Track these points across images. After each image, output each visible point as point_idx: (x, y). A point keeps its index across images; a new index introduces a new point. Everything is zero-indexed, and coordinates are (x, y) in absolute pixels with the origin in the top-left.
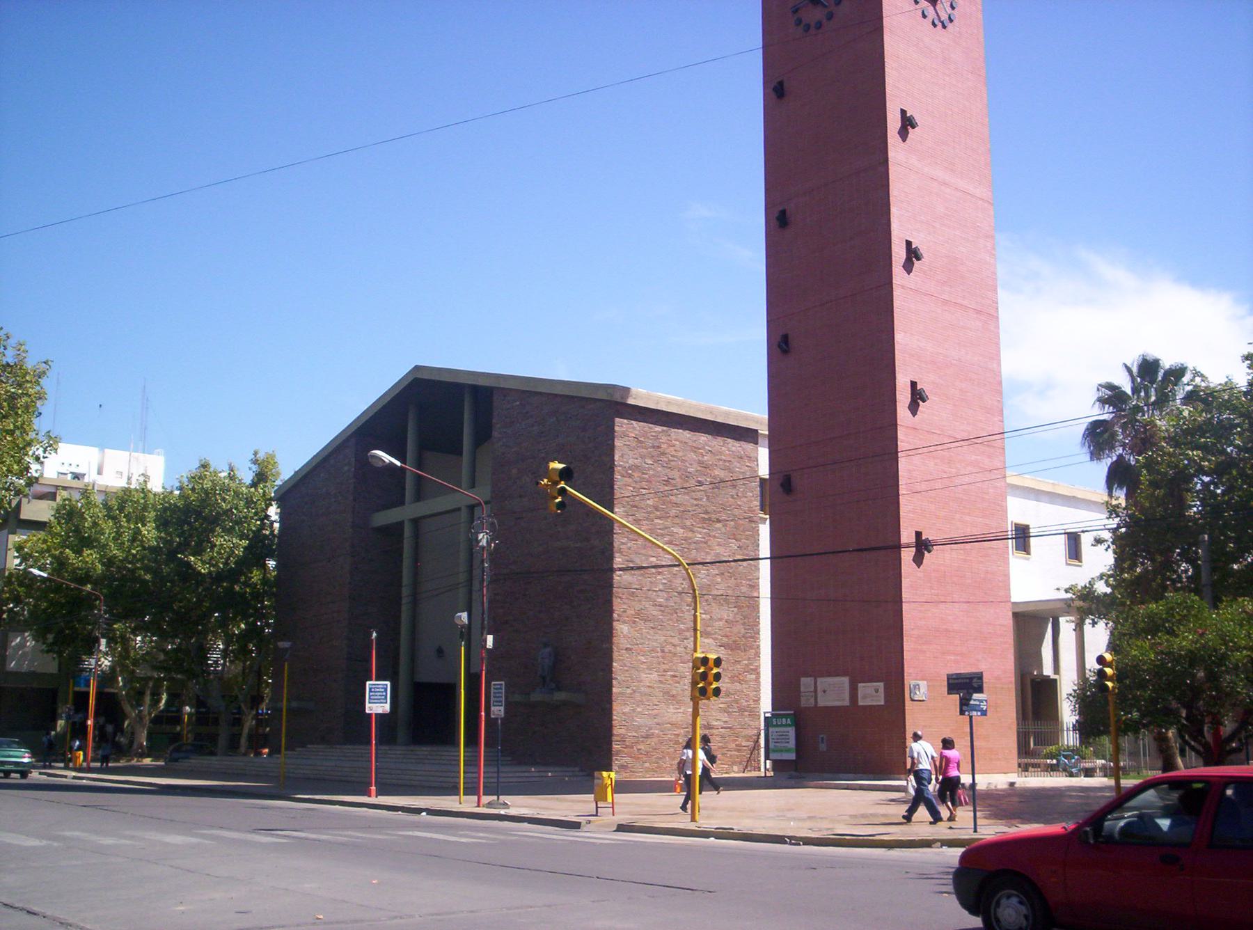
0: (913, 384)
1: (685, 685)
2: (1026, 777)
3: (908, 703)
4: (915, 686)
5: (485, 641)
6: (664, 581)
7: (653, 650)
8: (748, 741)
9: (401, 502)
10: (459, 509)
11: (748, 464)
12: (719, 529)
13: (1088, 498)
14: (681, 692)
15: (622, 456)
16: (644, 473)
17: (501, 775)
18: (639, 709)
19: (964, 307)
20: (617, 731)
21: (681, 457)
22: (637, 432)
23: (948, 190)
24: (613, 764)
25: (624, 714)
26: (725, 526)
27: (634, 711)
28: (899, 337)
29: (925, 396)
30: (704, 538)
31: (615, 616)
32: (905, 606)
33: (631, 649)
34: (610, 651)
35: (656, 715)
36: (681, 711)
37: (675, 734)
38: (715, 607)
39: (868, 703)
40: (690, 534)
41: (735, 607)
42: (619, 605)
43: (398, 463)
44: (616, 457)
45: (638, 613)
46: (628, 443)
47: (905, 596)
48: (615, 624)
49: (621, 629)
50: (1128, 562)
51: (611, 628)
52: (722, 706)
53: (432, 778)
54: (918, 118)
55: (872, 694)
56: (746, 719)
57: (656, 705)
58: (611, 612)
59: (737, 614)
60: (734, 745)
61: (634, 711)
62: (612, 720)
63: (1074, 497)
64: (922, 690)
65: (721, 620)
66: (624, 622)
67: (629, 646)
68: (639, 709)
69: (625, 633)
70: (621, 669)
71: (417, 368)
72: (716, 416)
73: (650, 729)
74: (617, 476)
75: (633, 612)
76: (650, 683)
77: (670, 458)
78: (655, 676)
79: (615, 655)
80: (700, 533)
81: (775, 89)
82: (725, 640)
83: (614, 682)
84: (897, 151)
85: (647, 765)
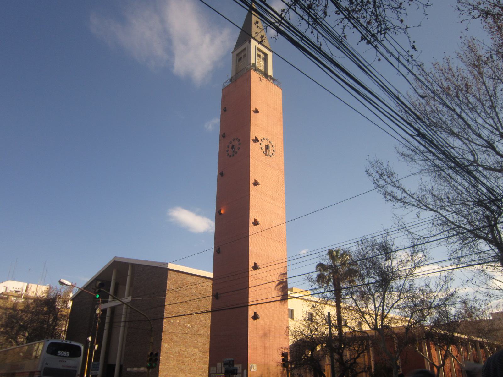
4: (252, 366)
6: (181, 329)
28: (250, 248)
31: (162, 340)
32: (249, 338)
38: (199, 339)
42: (164, 337)
47: (249, 334)
52: (200, 373)
65: (201, 342)
66: (166, 343)
71: (115, 257)
79: (161, 354)
81: (220, 174)
83: (160, 364)
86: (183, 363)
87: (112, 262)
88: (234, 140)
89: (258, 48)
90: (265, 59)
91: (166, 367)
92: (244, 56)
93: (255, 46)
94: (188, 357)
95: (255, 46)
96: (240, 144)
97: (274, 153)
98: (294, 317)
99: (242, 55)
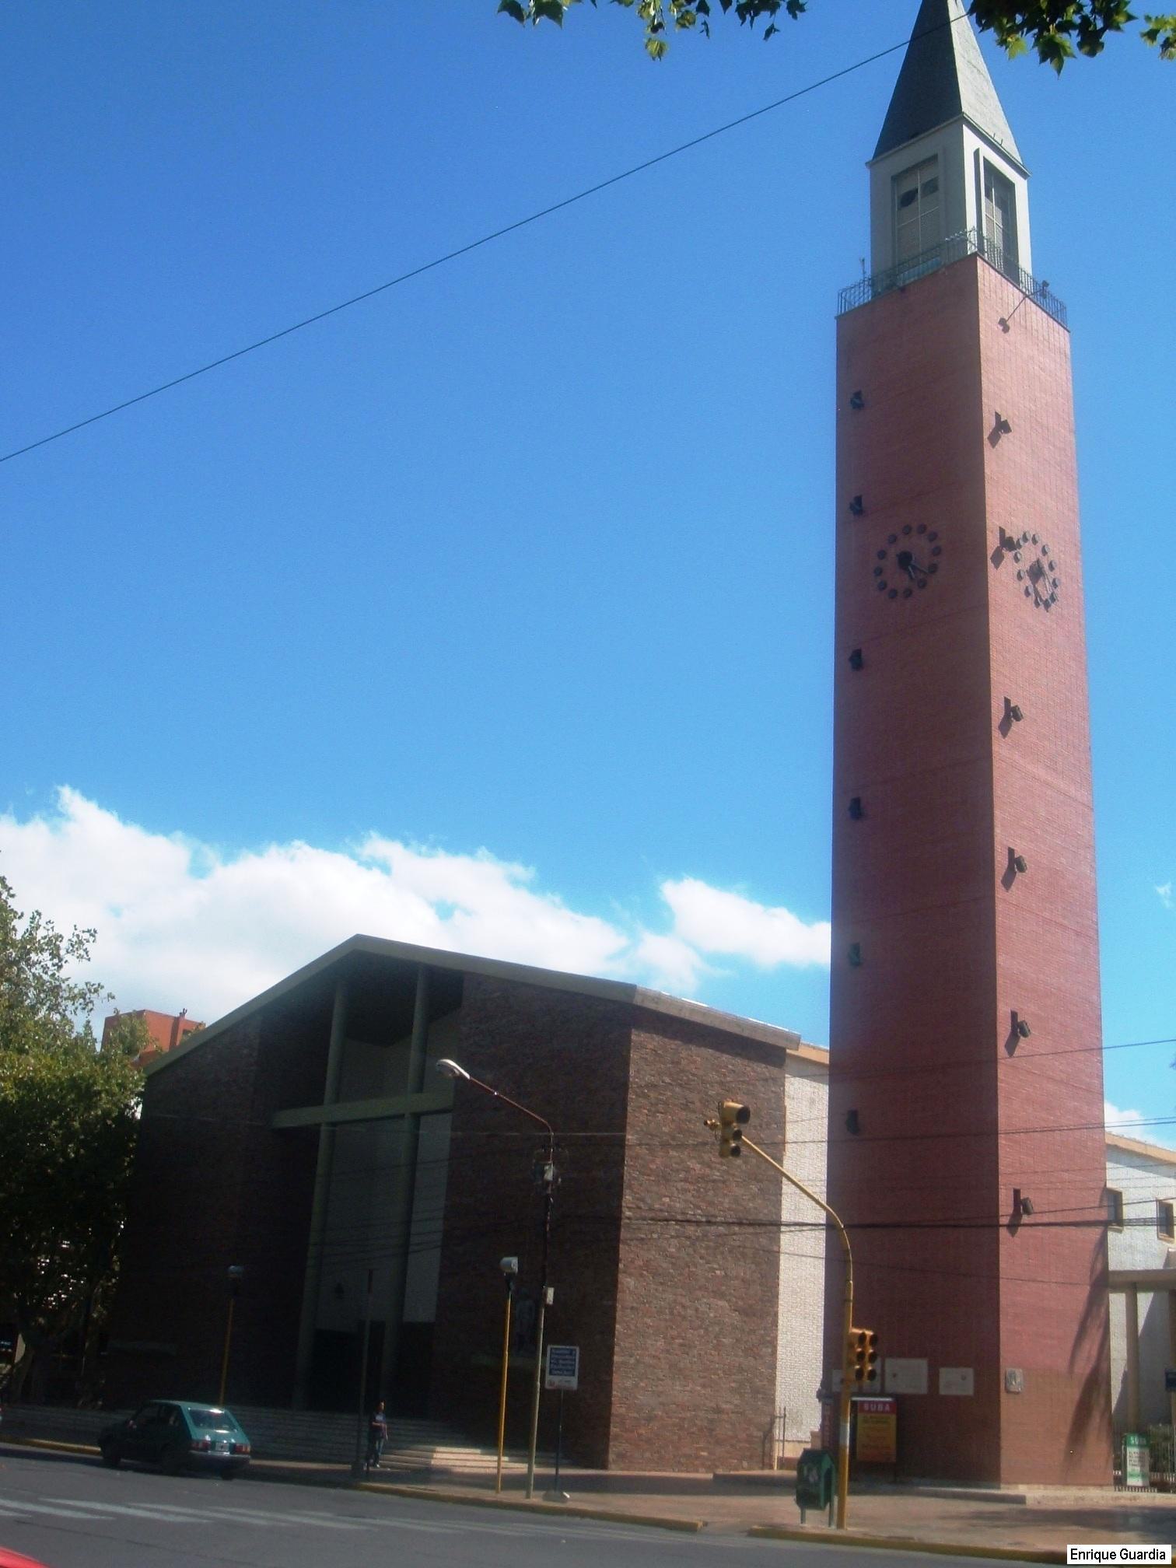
0: (1014, 1015)
1: (694, 1357)
2: (1119, 1490)
3: (1003, 1395)
5: (545, 1295)
7: (660, 1312)
8: (759, 1430)
9: (319, 1101)
10: (402, 1116)
11: (773, 1089)
12: (739, 1166)
13: (1130, 1148)
14: (689, 1365)
15: (638, 1071)
16: (660, 1094)
17: (496, 1464)
18: (642, 1384)
19: (1064, 927)
20: (618, 1409)
21: (702, 1076)
22: (655, 1044)
23: (1049, 792)
24: (610, 1451)
25: (626, 1389)
26: (746, 1163)
27: (636, 1385)
29: (1027, 1030)
30: (723, 1177)
31: (621, 1266)
33: (637, 1309)
34: (614, 1308)
35: (662, 1392)
36: (688, 1389)
37: (680, 1418)
39: (954, 1391)
40: (708, 1171)
41: (753, 1263)
43: (467, 1075)
44: (632, 1072)
45: (647, 1264)
46: (645, 1056)
48: (620, 1276)
49: (628, 1282)
50: (651, 1166)
51: (615, 1283)
52: (733, 1385)
53: (468, 1464)
54: (1024, 710)
55: (957, 1382)
56: (759, 1403)
57: (662, 1380)
58: (616, 1261)
59: (755, 1272)
60: (744, 1435)
61: (636, 1385)
62: (611, 1397)
63: (1116, 1146)
64: (1018, 1380)
65: (736, 1278)
66: (631, 1275)
67: (635, 1305)
68: (642, 1384)
69: (631, 1289)
70: (624, 1333)
71: (358, 939)
72: (743, 1030)
73: (653, 1409)
74: (631, 1096)
75: (641, 1263)
76: (656, 1351)
77: (691, 1077)
78: (660, 1343)
79: (619, 1314)
80: (718, 1170)
82: (740, 1303)
83: (616, 1349)
84: (1000, 747)
85: (647, 1455)
86: (686, 1347)
87: (770, 1040)
88: (907, 530)
89: (984, 158)
90: (1007, 205)
91: (632, 1361)
92: (931, 187)
93: (977, 153)
94: (700, 1327)
95: (977, 153)
96: (937, 552)
97: (1058, 591)
98: (1012, 1193)
99: (918, 181)
